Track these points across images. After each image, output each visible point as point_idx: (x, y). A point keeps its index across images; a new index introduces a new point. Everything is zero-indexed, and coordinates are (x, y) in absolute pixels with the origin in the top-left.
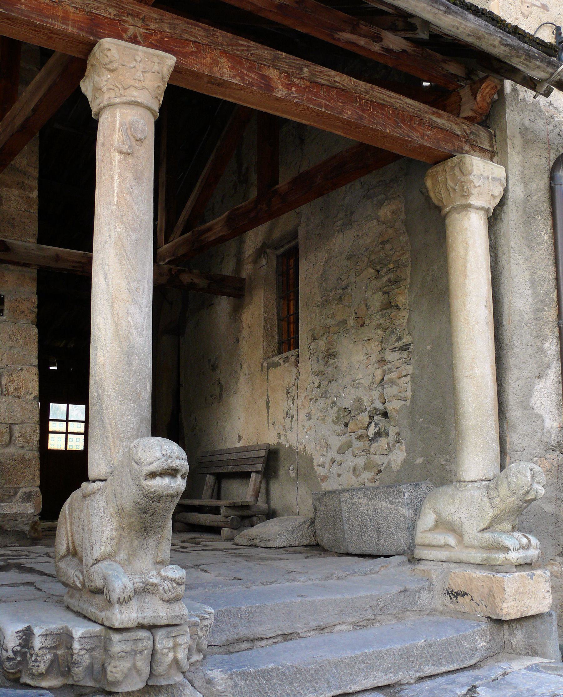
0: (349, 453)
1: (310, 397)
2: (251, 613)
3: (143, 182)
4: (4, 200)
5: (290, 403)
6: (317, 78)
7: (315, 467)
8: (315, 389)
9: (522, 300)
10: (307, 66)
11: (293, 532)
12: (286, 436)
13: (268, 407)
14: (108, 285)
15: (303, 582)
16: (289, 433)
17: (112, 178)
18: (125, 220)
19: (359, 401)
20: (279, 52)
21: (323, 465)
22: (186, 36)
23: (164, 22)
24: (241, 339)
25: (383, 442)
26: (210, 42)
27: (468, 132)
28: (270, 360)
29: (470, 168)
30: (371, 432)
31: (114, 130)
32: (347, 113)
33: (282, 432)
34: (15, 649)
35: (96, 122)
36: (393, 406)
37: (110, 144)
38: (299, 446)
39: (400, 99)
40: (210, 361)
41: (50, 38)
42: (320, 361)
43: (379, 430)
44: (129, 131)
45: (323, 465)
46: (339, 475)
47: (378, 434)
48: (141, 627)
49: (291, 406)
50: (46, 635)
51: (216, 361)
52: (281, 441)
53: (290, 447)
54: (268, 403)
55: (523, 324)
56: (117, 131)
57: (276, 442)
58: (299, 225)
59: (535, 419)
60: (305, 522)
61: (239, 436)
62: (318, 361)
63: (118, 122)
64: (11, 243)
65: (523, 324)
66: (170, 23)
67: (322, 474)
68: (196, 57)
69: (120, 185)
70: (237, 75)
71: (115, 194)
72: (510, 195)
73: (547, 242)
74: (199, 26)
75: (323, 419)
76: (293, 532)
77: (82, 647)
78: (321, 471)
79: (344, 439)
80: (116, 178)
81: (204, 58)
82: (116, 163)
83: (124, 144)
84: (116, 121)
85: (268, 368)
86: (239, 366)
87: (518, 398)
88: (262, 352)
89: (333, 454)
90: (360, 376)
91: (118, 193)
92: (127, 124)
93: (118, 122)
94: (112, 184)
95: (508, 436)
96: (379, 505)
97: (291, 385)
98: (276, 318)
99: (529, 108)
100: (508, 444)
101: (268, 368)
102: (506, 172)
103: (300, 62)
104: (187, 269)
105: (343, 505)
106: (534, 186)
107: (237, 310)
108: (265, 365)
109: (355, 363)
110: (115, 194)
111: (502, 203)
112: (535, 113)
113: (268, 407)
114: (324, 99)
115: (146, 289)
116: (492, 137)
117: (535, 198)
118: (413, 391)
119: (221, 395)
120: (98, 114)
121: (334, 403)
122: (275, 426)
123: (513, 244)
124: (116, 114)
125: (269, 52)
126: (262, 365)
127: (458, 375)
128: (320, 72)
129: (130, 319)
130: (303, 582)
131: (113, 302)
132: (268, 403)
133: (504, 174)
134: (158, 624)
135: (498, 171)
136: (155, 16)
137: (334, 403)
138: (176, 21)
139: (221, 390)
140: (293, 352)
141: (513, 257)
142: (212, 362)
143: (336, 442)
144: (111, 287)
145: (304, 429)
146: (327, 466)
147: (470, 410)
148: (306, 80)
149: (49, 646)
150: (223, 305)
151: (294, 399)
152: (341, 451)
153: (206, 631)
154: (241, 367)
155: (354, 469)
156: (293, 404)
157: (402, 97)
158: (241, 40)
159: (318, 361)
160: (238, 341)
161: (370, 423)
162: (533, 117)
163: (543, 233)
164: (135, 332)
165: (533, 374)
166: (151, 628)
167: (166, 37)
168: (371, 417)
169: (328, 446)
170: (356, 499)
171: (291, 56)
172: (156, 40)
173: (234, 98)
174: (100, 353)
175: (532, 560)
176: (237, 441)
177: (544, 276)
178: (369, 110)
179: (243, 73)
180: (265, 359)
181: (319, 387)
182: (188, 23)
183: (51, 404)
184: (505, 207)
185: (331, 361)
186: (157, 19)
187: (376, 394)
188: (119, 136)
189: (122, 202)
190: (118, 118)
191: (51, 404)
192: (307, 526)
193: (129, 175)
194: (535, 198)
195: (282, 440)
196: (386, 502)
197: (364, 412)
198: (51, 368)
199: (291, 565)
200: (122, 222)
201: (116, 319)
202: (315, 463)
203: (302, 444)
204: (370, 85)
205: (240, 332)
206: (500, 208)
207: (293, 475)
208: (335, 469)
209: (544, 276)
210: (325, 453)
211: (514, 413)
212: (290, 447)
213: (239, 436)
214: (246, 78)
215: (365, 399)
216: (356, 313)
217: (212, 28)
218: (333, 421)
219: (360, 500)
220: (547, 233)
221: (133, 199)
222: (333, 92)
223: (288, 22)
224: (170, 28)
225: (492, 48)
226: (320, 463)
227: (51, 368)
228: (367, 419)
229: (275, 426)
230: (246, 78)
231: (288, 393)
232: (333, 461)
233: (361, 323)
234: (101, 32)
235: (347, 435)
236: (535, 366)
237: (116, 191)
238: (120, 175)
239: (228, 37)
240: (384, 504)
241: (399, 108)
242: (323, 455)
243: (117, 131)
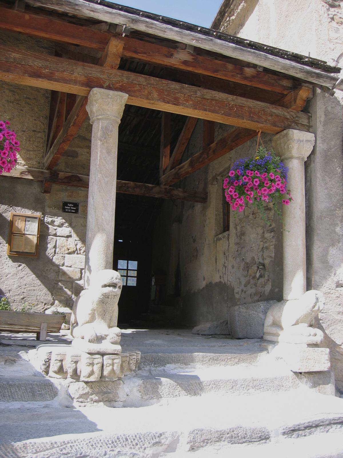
0: (249, 286)
1: (234, 256)
2: (164, 358)
3: (111, 155)
4: (79, 154)
5: (225, 260)
6: (205, 96)
7: (235, 294)
8: (236, 252)
9: (321, 204)
10: (199, 90)
11: (217, 327)
12: (223, 277)
13: (216, 262)
14: (94, 202)
15: (199, 347)
16: (224, 276)
17: (97, 153)
18: (102, 172)
19: (253, 258)
20: (184, 85)
21: (238, 293)
22: (135, 82)
23: (123, 76)
24: (205, 225)
25: (262, 280)
26: (147, 84)
27: (295, 116)
28: (217, 237)
29: (292, 136)
30: (258, 275)
31: (98, 130)
32: (221, 112)
33: (222, 276)
34: (46, 360)
35: (92, 125)
36: (267, 262)
37: (97, 137)
38: (228, 282)
39: (253, 102)
40: (193, 237)
41: (70, 89)
42: (238, 237)
43: (261, 274)
44: (105, 131)
45: (238, 293)
46: (245, 298)
47: (261, 276)
48: (98, 353)
49: (226, 261)
50: (58, 355)
51: (195, 237)
52: (221, 280)
53: (225, 283)
54: (216, 259)
55: (323, 218)
56: (100, 131)
57: (219, 281)
58: (231, 164)
59: (329, 269)
60: (224, 322)
61: (204, 278)
62: (237, 237)
63: (100, 126)
64: (81, 177)
65: (323, 218)
66: (127, 77)
67: (238, 297)
68: (140, 92)
69: (100, 156)
70: (161, 98)
71: (98, 160)
72: (318, 149)
73: (340, 174)
74: (141, 77)
75: (239, 269)
76: (217, 327)
77: (72, 360)
78: (237, 296)
79: (247, 279)
80: (99, 153)
81: (144, 92)
82: (99, 146)
83: (102, 137)
84: (99, 126)
85: (216, 241)
86: (205, 240)
87: (319, 257)
88: (214, 232)
89: (242, 287)
90: (254, 245)
91: (99, 160)
92: (104, 127)
93: (100, 126)
94: (97, 156)
95: (313, 277)
96: (251, 313)
97: (226, 250)
98: (222, 214)
99: (331, 101)
100: (313, 281)
101: (216, 241)
102: (316, 137)
103: (195, 88)
104: (175, 188)
105: (236, 313)
106: (333, 143)
107: (204, 209)
108: (215, 239)
109: (252, 238)
110: (98, 160)
111: (313, 152)
112: (335, 103)
113: (216, 262)
114: (208, 106)
115: (111, 204)
116: (309, 118)
117: (333, 150)
118: (275, 253)
119: (197, 255)
120: (93, 122)
121: (243, 259)
122: (219, 272)
123: (318, 175)
124: (99, 123)
125: (178, 85)
126: (214, 239)
127: (284, 244)
128: (207, 93)
129: (103, 217)
130: (199, 347)
131: (96, 210)
132: (216, 259)
133: (314, 138)
134: (107, 353)
135: (310, 136)
136: (119, 74)
137: (243, 259)
138: (130, 75)
139: (197, 253)
140: (227, 232)
141: (318, 182)
142: (194, 238)
143: (244, 281)
144: (95, 202)
145: (231, 273)
146: (240, 293)
147: (289, 263)
148: (198, 97)
149: (59, 360)
150: (198, 207)
151: (226, 258)
152: (245, 286)
153: (135, 361)
154: (206, 240)
155: (251, 295)
156: (226, 260)
157: (254, 101)
158: (164, 81)
159: (237, 237)
160: (204, 226)
161: (257, 270)
162: (334, 105)
163: (337, 169)
164: (105, 223)
165: (328, 244)
166: (103, 354)
167: (124, 84)
168: (258, 267)
169: (240, 282)
170: (241, 310)
171: (191, 86)
172: (120, 86)
173: (162, 109)
174: (90, 233)
175: (317, 343)
176: (203, 280)
177: (337, 192)
178: (234, 110)
179: (164, 97)
180: (215, 236)
181: (237, 251)
182: (136, 76)
183: (119, 260)
184: (315, 155)
185: (243, 237)
186: (120, 75)
187: (260, 254)
188: (101, 133)
189: (101, 164)
190: (100, 125)
191: (119, 260)
192: (224, 324)
193: (104, 151)
194: (333, 150)
195: (222, 280)
196: (253, 311)
197: (255, 264)
198: (119, 241)
199: (212, 344)
200: (101, 173)
201: (97, 217)
202: (235, 291)
203: (230, 282)
204: (235, 96)
205: (205, 221)
206: (313, 156)
207: (226, 298)
208: (243, 295)
209: (337, 192)
210: (239, 286)
211: (316, 265)
212: (225, 283)
213: (204, 278)
214: (166, 99)
215: (256, 258)
216: (253, 212)
217: (148, 77)
218: (242, 269)
219: (243, 310)
220: (340, 168)
221: (106, 162)
222: (214, 102)
223: (190, 69)
224: (127, 79)
225: (296, 74)
226: (237, 292)
227: (119, 241)
228: (256, 268)
229: (219, 272)
230: (166, 99)
231: (225, 254)
232: (242, 291)
233: (255, 217)
234: (92, 85)
235: (248, 277)
236: (330, 240)
237: (98, 159)
238: (101, 151)
239: (157, 80)
240: (253, 312)
241: (252, 107)
242: (238, 288)
243: (100, 131)
